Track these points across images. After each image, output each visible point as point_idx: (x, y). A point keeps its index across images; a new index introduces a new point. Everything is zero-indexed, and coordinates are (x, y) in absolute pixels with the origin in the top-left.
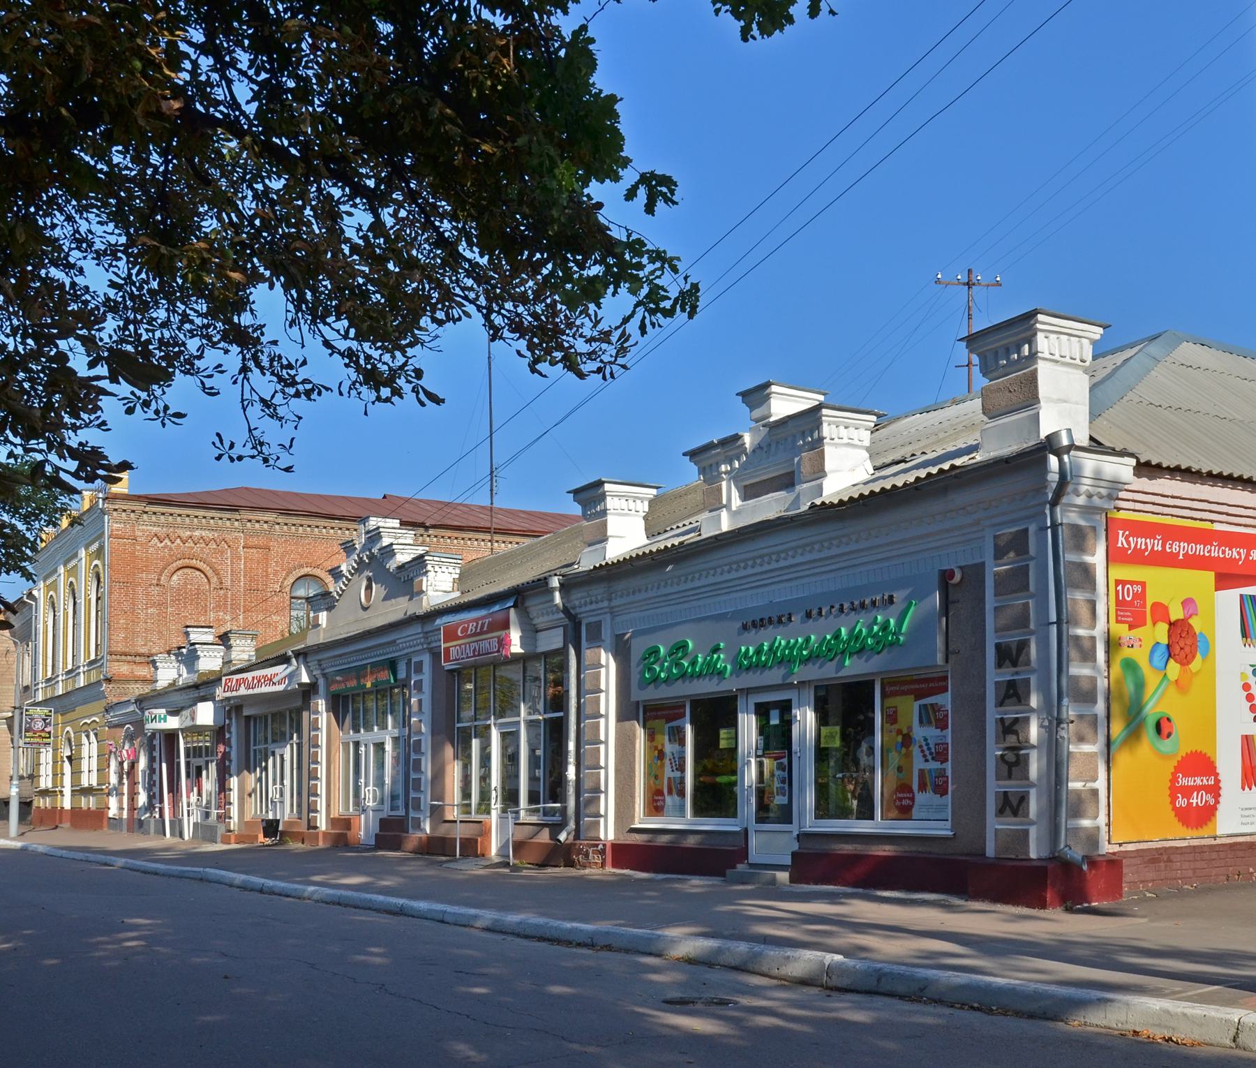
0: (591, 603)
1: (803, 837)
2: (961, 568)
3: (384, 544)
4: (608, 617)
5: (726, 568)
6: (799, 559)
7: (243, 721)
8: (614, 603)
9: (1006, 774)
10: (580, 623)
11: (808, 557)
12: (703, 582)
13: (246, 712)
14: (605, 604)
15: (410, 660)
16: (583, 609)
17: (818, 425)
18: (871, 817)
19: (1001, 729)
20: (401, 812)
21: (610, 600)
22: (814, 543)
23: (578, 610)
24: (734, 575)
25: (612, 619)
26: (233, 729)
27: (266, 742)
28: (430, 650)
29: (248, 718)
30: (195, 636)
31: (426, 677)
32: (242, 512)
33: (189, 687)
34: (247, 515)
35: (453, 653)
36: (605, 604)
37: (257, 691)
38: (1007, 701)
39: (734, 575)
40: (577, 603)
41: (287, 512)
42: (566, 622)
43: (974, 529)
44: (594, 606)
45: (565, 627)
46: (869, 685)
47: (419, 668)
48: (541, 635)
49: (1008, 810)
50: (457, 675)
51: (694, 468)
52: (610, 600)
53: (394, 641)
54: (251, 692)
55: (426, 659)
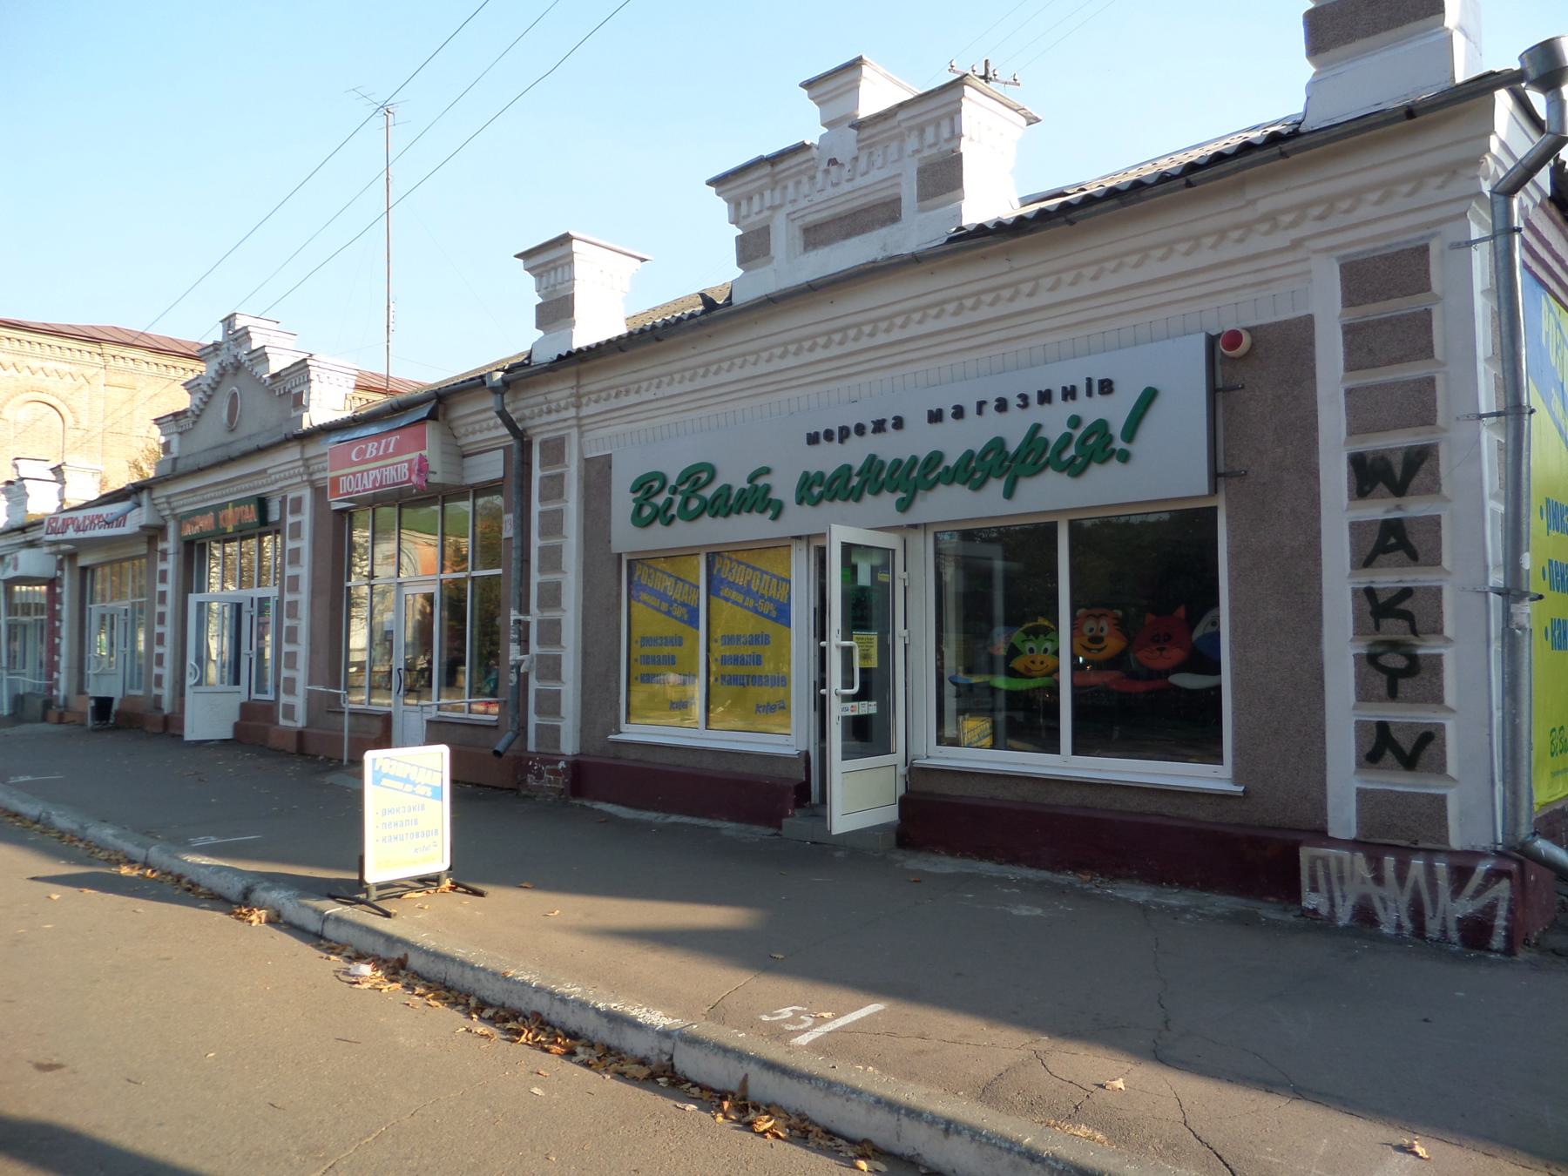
0: (549, 412)
1: (916, 773)
2: (1248, 330)
3: (254, 347)
4: (574, 432)
5: (778, 351)
6: (914, 330)
7: (77, 572)
8: (584, 412)
9: (1383, 691)
10: (530, 444)
11: (932, 325)
12: (736, 374)
13: (83, 561)
14: (572, 412)
15: (285, 498)
16: (537, 421)
17: (955, 113)
18: (1055, 749)
19: (1368, 607)
20: (270, 697)
21: (578, 406)
22: (944, 302)
23: (529, 423)
24: (790, 361)
25: (581, 435)
26: (66, 582)
27: (279, 603)
28: (312, 483)
29: (84, 569)
30: (26, 469)
31: (306, 518)
32: (104, 345)
33: (14, 530)
34: (109, 349)
35: (344, 486)
36: (572, 412)
37: (89, 534)
38: (1381, 558)
39: (790, 361)
40: (527, 412)
41: (158, 351)
42: (510, 441)
43: (1289, 257)
44: (554, 417)
45: (507, 449)
46: (1052, 529)
47: (297, 506)
48: (469, 461)
49: (1389, 756)
50: (344, 518)
51: (814, 110)
52: (578, 406)
53: (265, 471)
54: (81, 535)
55: (307, 494)
